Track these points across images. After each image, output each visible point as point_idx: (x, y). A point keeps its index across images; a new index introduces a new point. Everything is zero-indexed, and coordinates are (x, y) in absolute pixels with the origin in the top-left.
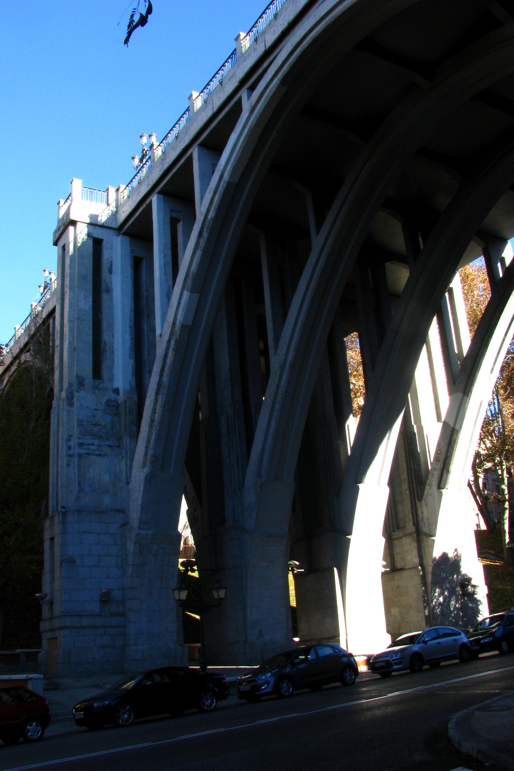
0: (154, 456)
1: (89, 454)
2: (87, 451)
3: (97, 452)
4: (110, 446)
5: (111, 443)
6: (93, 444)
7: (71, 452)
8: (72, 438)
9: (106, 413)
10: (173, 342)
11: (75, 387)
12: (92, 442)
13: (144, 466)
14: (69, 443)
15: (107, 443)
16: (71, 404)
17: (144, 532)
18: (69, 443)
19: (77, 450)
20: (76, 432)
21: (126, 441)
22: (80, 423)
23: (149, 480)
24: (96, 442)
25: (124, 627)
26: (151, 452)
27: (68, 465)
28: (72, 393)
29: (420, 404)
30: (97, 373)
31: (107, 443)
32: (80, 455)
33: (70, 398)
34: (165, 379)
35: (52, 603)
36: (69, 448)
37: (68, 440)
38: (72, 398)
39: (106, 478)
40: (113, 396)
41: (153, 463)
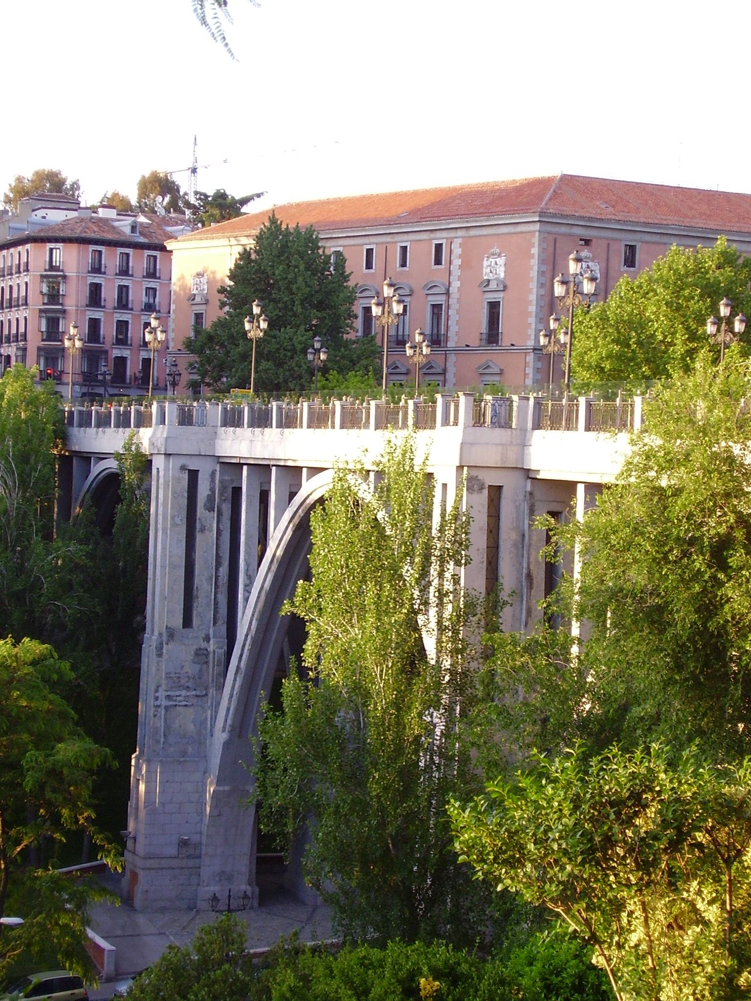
0: (232, 726)
1: (176, 706)
2: (174, 703)
3: (184, 703)
4: (197, 696)
5: (198, 693)
6: (180, 696)
7: (158, 703)
8: (160, 689)
9: (195, 663)
10: (249, 637)
11: (165, 638)
12: (178, 693)
13: (223, 731)
14: (157, 694)
15: (194, 693)
16: (160, 655)
17: (221, 788)
18: (157, 694)
19: (164, 703)
20: (164, 682)
21: (212, 691)
22: (168, 677)
23: (227, 745)
24: (184, 693)
25: (199, 868)
26: (229, 722)
27: (155, 716)
28: (161, 644)
29: (714, 188)
30: (187, 622)
31: (194, 693)
32: (167, 708)
33: (160, 648)
34: (243, 664)
35: (135, 839)
36: (157, 698)
37: (157, 691)
38: (162, 648)
39: (191, 727)
40: (204, 645)
41: (231, 731)
